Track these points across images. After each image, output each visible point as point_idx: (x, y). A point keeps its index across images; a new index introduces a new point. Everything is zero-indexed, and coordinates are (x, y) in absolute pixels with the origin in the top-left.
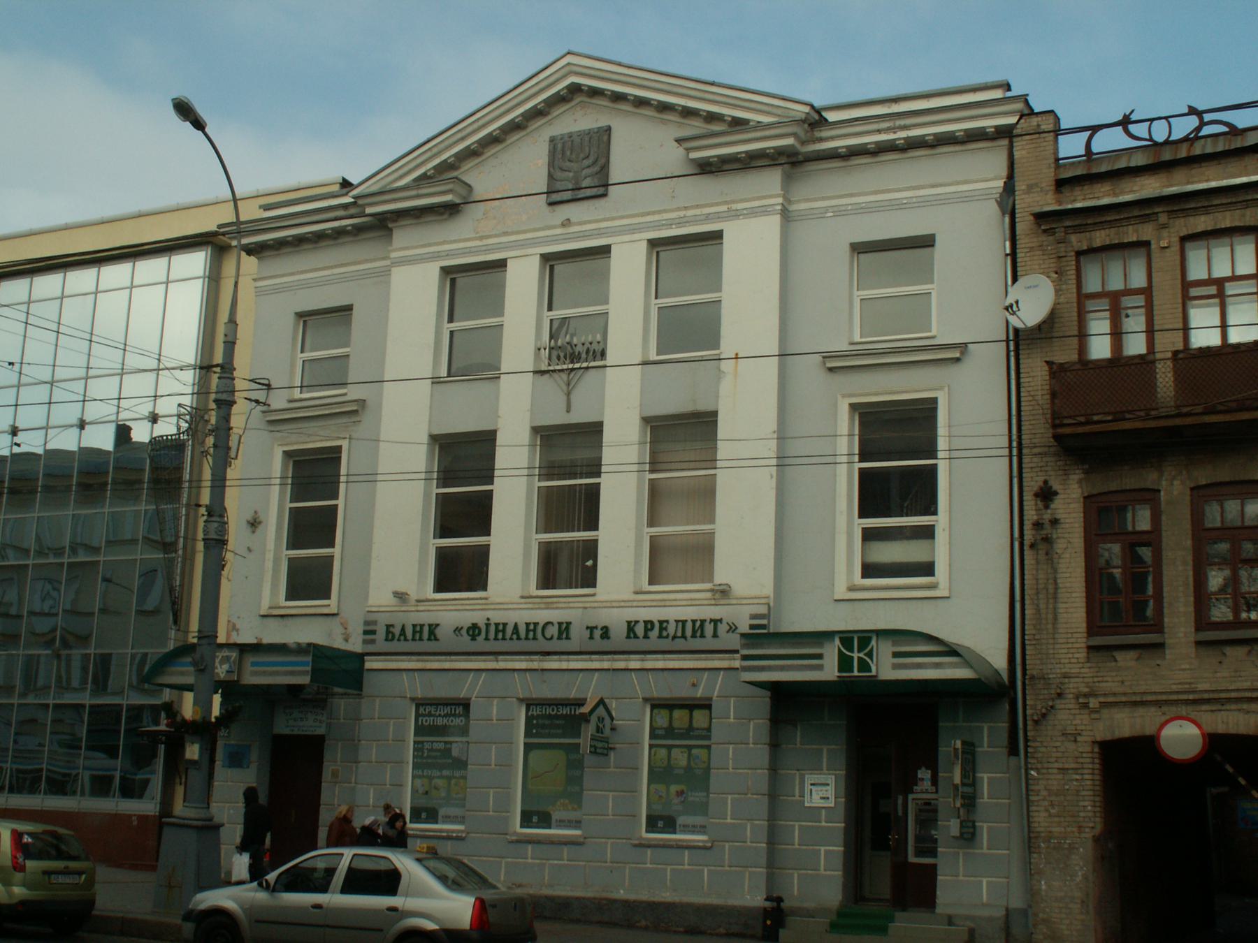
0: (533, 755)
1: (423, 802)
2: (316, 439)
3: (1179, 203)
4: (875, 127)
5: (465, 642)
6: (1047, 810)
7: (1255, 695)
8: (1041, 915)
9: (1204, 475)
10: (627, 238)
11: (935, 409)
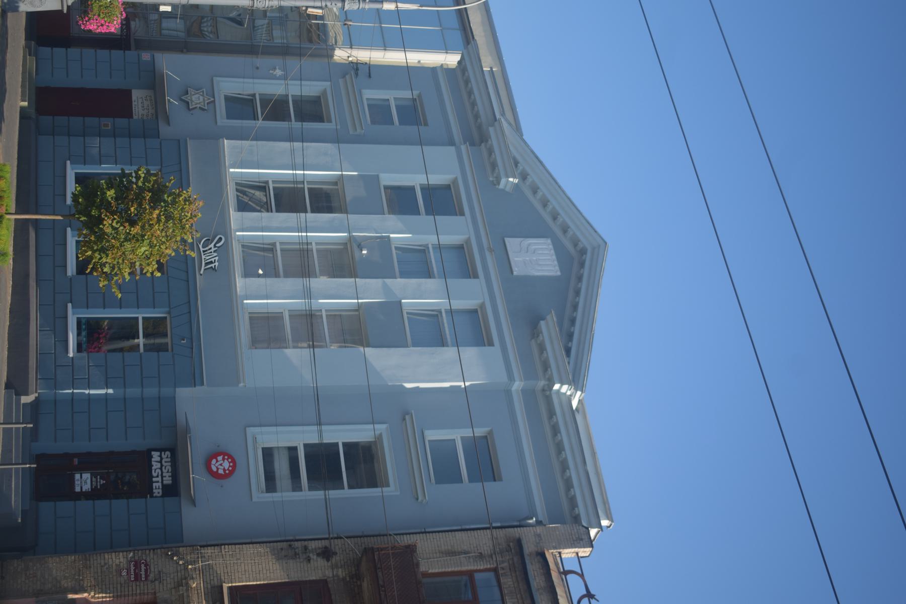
6: (105, 564)
8: (31, 564)
11: (369, 486)
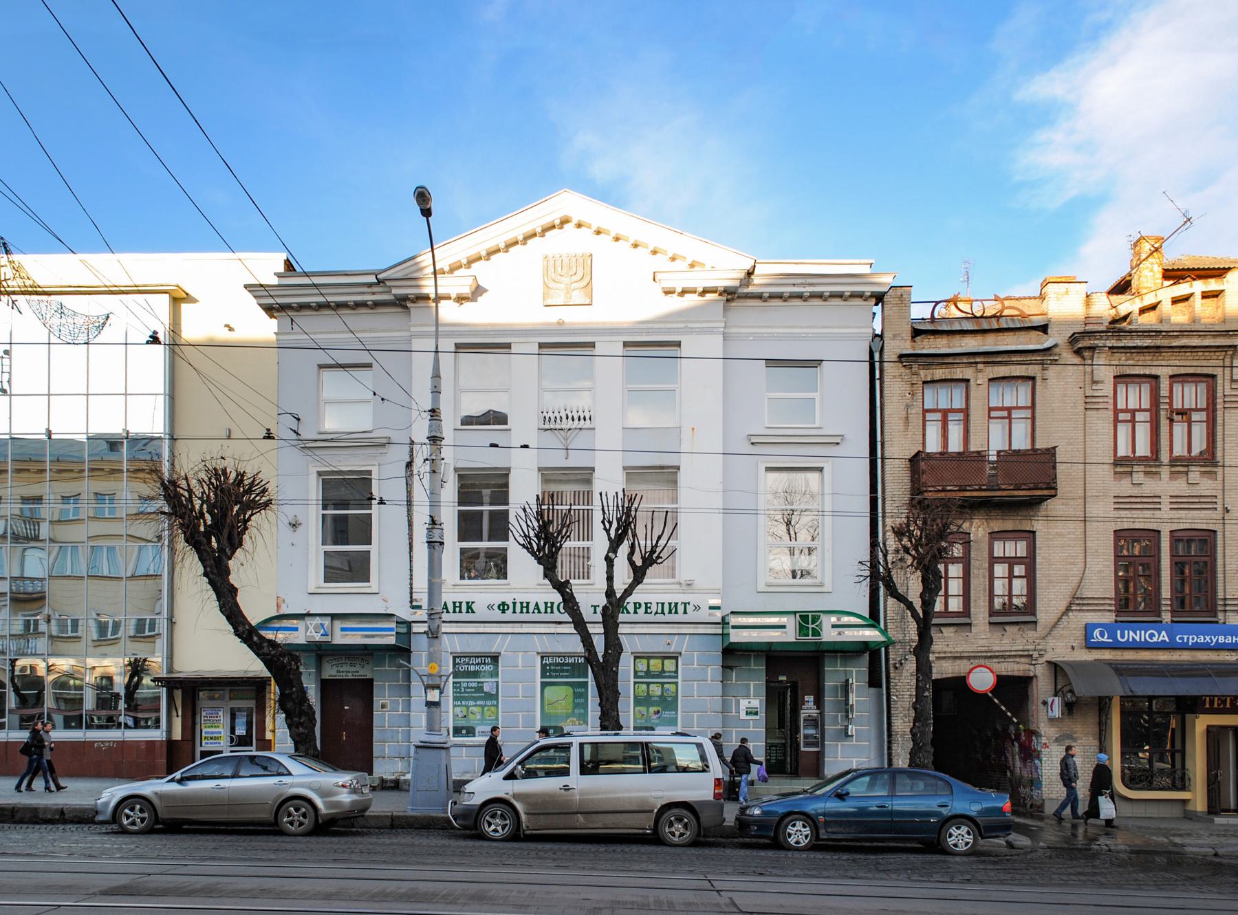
0: (548, 690)
1: (462, 723)
2: (348, 463)
3: (991, 356)
4: (792, 281)
5: (497, 615)
7: (1231, 657)
9: (997, 525)
10: (608, 338)
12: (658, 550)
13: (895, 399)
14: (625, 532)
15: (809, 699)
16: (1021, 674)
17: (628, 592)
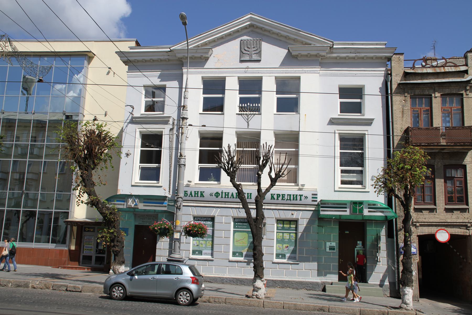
0: (236, 234)
1: (196, 248)
12: (282, 171)
13: (398, 103)
14: (266, 163)
15: (359, 243)
16: (462, 234)
17: (268, 190)
